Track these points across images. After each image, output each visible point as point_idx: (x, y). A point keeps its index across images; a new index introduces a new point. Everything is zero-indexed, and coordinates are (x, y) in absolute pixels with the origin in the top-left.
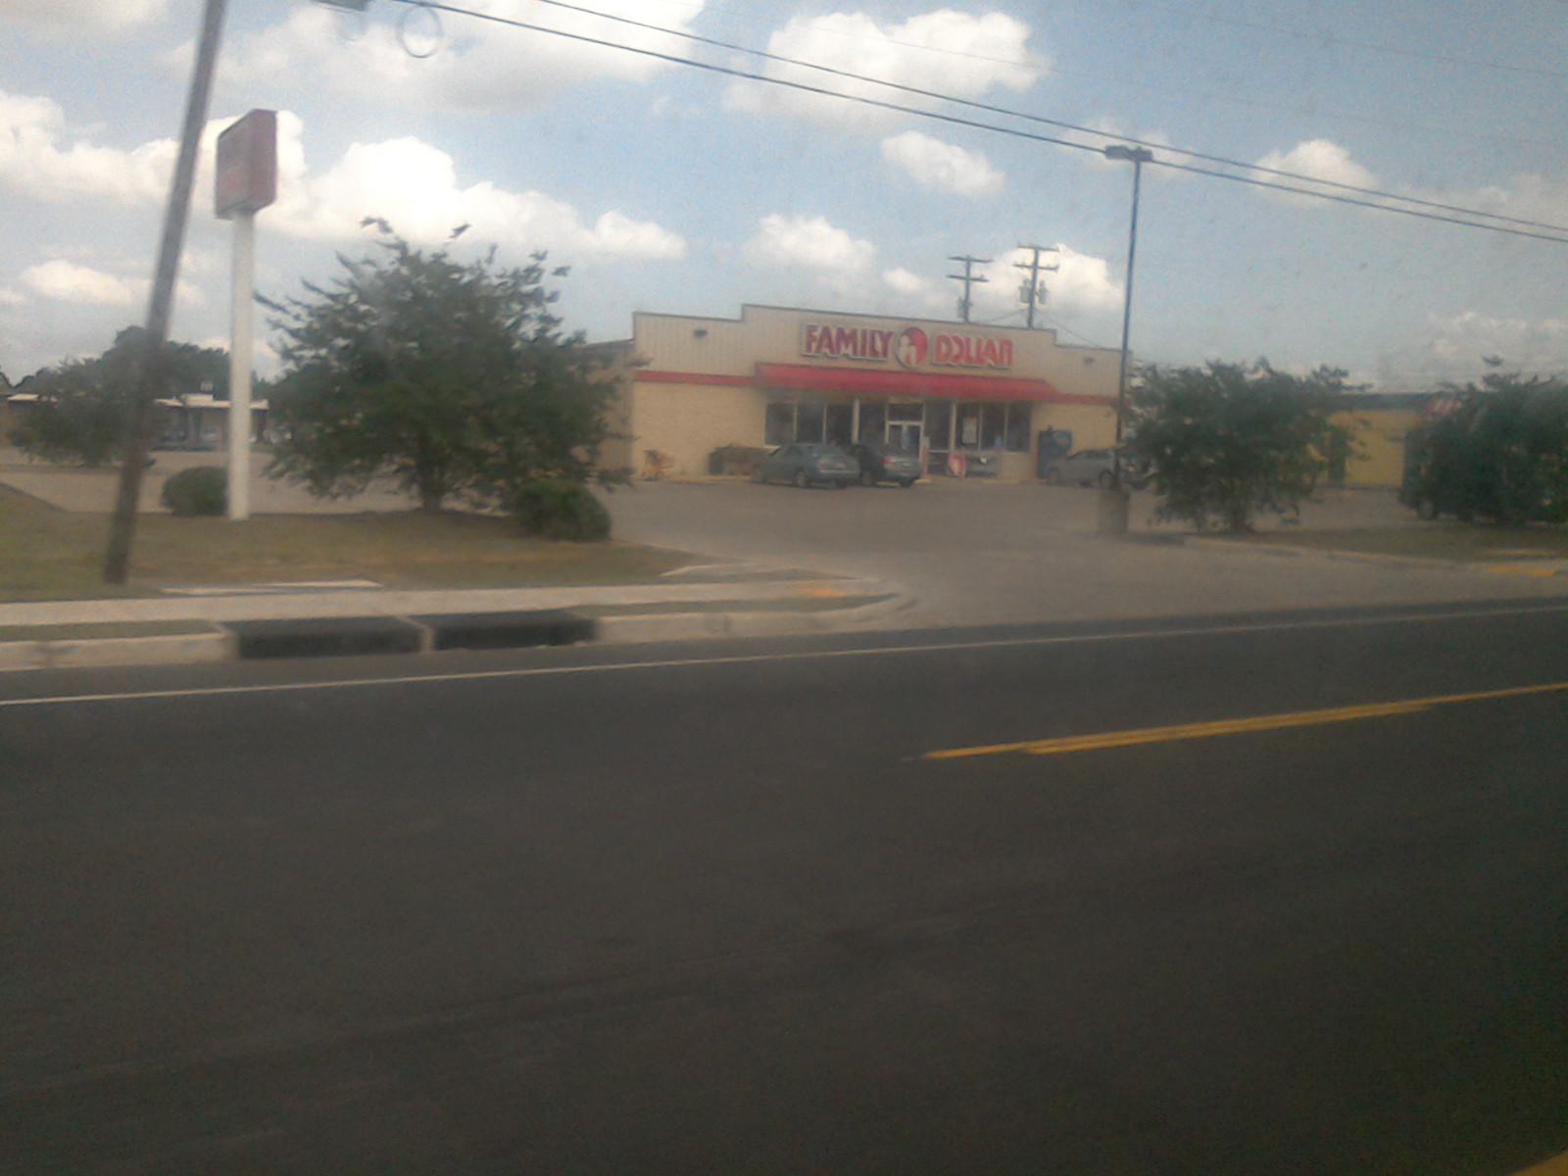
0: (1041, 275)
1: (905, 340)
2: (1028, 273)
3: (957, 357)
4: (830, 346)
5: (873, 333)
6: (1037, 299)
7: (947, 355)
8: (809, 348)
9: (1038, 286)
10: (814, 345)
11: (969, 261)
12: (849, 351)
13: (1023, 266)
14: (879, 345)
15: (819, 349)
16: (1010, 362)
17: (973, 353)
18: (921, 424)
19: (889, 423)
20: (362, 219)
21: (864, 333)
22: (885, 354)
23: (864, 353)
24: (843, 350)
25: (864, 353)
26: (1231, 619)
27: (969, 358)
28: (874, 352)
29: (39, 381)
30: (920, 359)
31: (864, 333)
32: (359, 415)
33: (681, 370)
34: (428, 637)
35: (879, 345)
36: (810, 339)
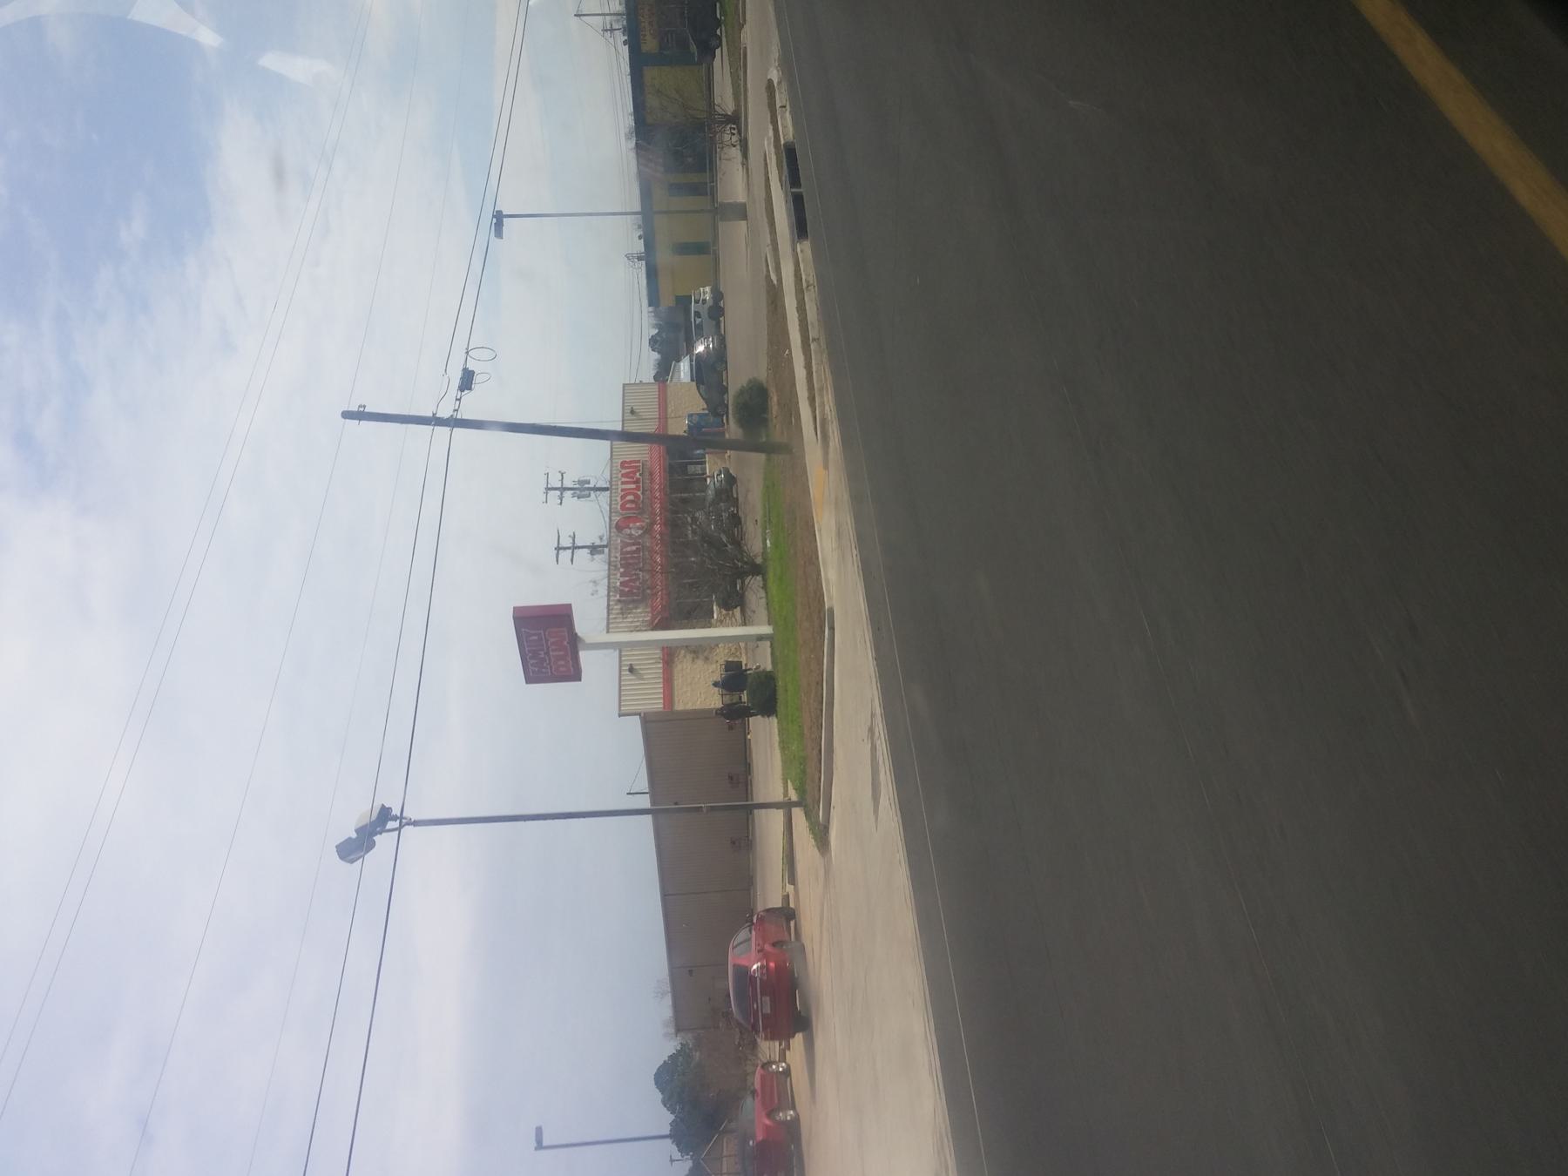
0: (568, 484)
17: (633, 486)
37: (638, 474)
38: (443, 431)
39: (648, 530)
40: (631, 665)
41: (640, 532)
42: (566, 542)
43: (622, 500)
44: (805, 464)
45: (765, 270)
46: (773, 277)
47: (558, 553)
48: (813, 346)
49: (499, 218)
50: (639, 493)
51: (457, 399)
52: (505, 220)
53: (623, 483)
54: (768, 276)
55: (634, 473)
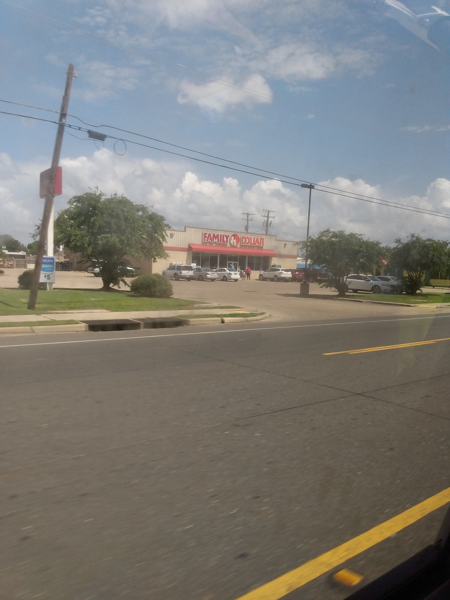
0: (270, 219)
1: (233, 238)
2: (266, 219)
3: (247, 243)
4: (211, 239)
5: (223, 235)
6: (269, 226)
7: (245, 243)
8: (205, 240)
9: (269, 222)
10: (206, 239)
11: (248, 214)
12: (217, 241)
13: (265, 216)
14: (225, 239)
15: (207, 240)
16: (263, 245)
17: (252, 242)
18: (238, 263)
19: (228, 262)
20: (89, 187)
21: (221, 235)
22: (227, 242)
23: (221, 242)
24: (215, 240)
25: (221, 242)
26: (330, 321)
27: (251, 244)
28: (224, 241)
29: (3, 236)
30: (237, 243)
31: (221, 235)
32: (93, 238)
33: (310, 217)
34: (142, 326)
35: (225, 239)
36: (205, 237)
37: (258, 244)
38: (57, 118)
39: (232, 246)
40: (287, 245)
41: (232, 243)
42: (250, 217)
43: (246, 237)
44: (144, 311)
45: (211, 303)
46: (196, 306)
47: (247, 214)
48: (28, 328)
49: (311, 187)
50: (249, 244)
51: (80, 130)
52: (309, 189)
53: (254, 238)
54: (197, 303)
55: (258, 243)
